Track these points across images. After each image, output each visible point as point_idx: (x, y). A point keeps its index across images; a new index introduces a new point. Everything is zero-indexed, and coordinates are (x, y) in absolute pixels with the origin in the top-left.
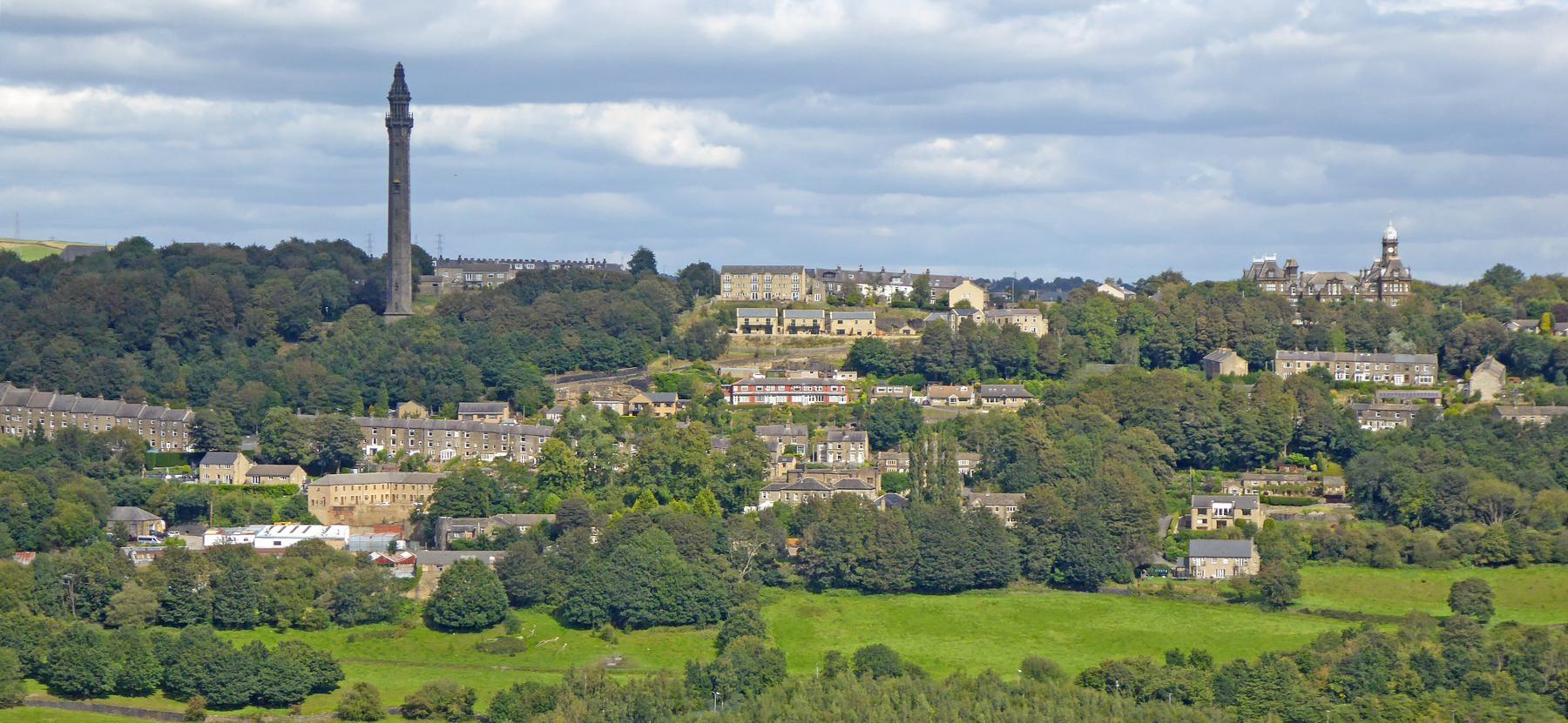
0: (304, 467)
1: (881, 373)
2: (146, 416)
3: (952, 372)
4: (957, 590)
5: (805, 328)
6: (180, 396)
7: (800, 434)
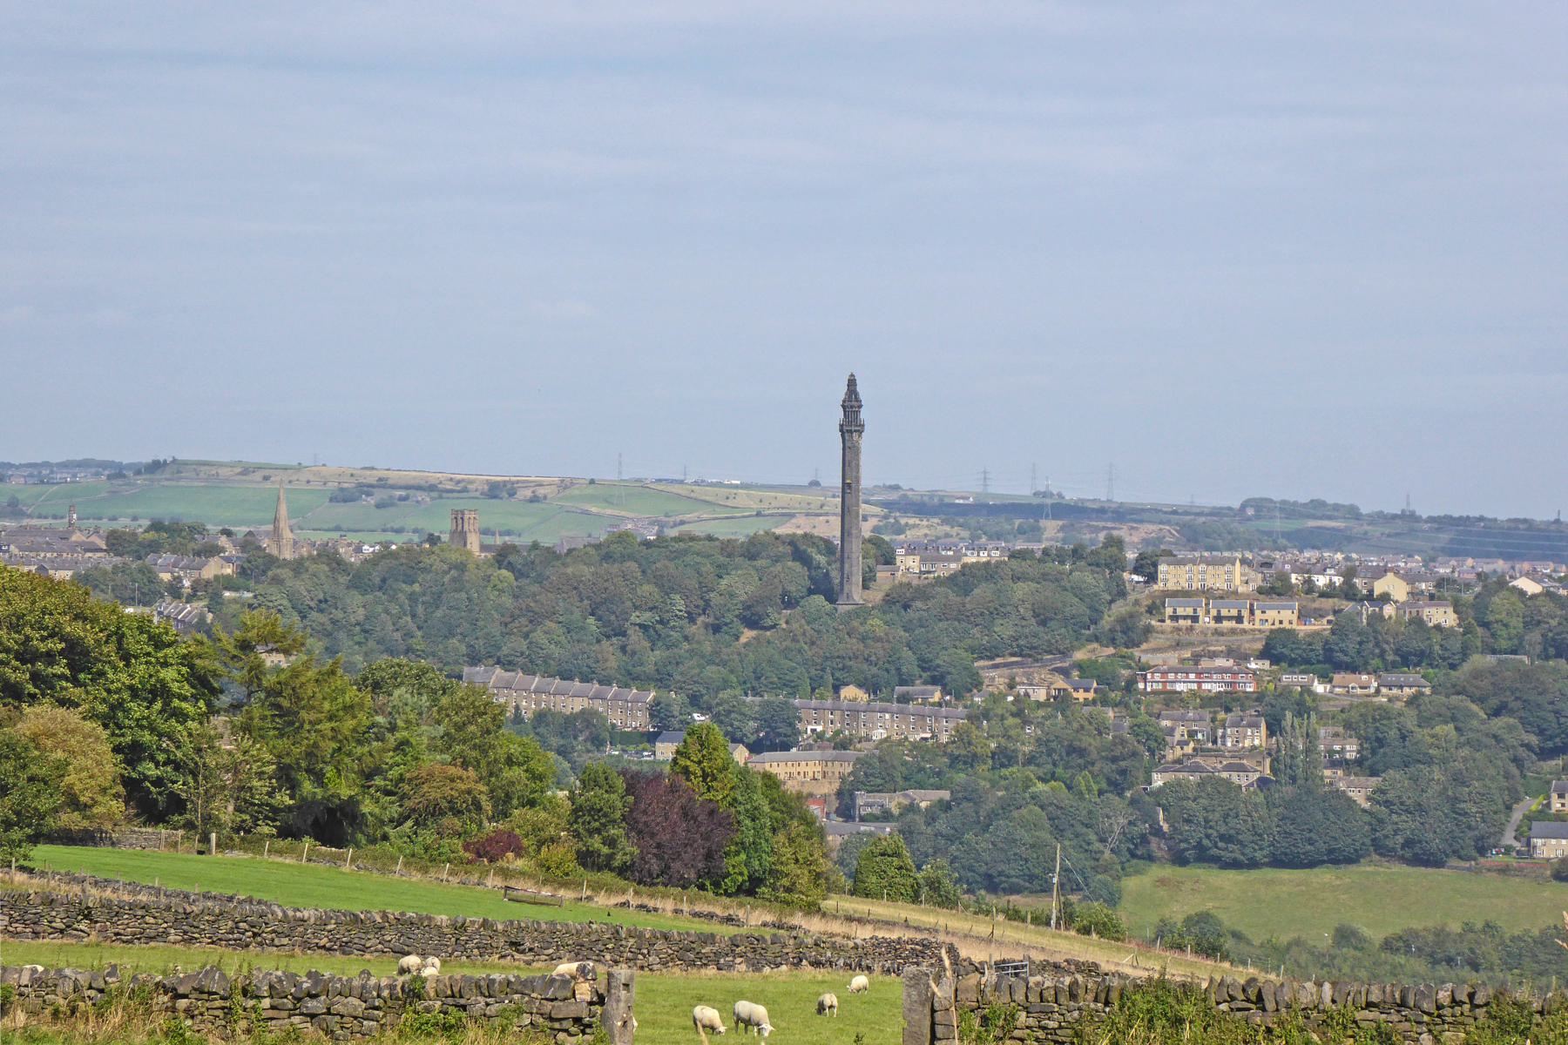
0: (748, 746)
1: (1292, 663)
2: (615, 698)
3: (1359, 661)
4: (1311, 865)
5: (1229, 618)
6: (649, 679)
7: (1202, 719)
